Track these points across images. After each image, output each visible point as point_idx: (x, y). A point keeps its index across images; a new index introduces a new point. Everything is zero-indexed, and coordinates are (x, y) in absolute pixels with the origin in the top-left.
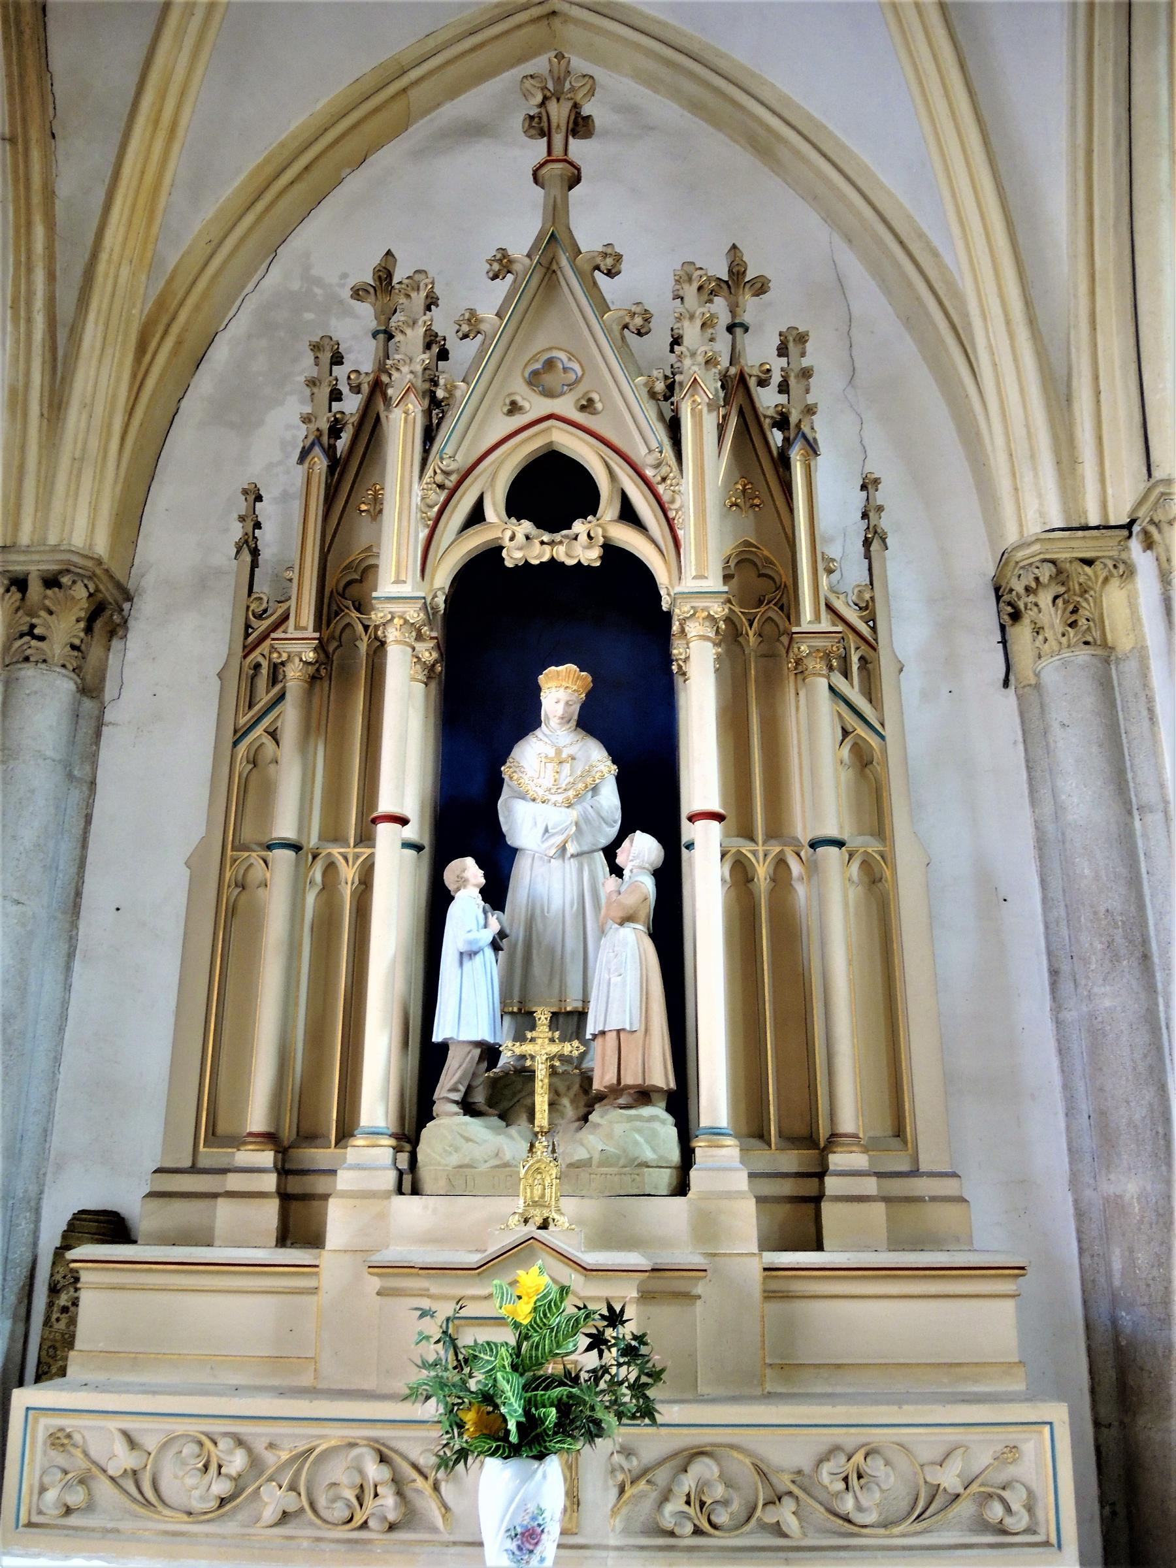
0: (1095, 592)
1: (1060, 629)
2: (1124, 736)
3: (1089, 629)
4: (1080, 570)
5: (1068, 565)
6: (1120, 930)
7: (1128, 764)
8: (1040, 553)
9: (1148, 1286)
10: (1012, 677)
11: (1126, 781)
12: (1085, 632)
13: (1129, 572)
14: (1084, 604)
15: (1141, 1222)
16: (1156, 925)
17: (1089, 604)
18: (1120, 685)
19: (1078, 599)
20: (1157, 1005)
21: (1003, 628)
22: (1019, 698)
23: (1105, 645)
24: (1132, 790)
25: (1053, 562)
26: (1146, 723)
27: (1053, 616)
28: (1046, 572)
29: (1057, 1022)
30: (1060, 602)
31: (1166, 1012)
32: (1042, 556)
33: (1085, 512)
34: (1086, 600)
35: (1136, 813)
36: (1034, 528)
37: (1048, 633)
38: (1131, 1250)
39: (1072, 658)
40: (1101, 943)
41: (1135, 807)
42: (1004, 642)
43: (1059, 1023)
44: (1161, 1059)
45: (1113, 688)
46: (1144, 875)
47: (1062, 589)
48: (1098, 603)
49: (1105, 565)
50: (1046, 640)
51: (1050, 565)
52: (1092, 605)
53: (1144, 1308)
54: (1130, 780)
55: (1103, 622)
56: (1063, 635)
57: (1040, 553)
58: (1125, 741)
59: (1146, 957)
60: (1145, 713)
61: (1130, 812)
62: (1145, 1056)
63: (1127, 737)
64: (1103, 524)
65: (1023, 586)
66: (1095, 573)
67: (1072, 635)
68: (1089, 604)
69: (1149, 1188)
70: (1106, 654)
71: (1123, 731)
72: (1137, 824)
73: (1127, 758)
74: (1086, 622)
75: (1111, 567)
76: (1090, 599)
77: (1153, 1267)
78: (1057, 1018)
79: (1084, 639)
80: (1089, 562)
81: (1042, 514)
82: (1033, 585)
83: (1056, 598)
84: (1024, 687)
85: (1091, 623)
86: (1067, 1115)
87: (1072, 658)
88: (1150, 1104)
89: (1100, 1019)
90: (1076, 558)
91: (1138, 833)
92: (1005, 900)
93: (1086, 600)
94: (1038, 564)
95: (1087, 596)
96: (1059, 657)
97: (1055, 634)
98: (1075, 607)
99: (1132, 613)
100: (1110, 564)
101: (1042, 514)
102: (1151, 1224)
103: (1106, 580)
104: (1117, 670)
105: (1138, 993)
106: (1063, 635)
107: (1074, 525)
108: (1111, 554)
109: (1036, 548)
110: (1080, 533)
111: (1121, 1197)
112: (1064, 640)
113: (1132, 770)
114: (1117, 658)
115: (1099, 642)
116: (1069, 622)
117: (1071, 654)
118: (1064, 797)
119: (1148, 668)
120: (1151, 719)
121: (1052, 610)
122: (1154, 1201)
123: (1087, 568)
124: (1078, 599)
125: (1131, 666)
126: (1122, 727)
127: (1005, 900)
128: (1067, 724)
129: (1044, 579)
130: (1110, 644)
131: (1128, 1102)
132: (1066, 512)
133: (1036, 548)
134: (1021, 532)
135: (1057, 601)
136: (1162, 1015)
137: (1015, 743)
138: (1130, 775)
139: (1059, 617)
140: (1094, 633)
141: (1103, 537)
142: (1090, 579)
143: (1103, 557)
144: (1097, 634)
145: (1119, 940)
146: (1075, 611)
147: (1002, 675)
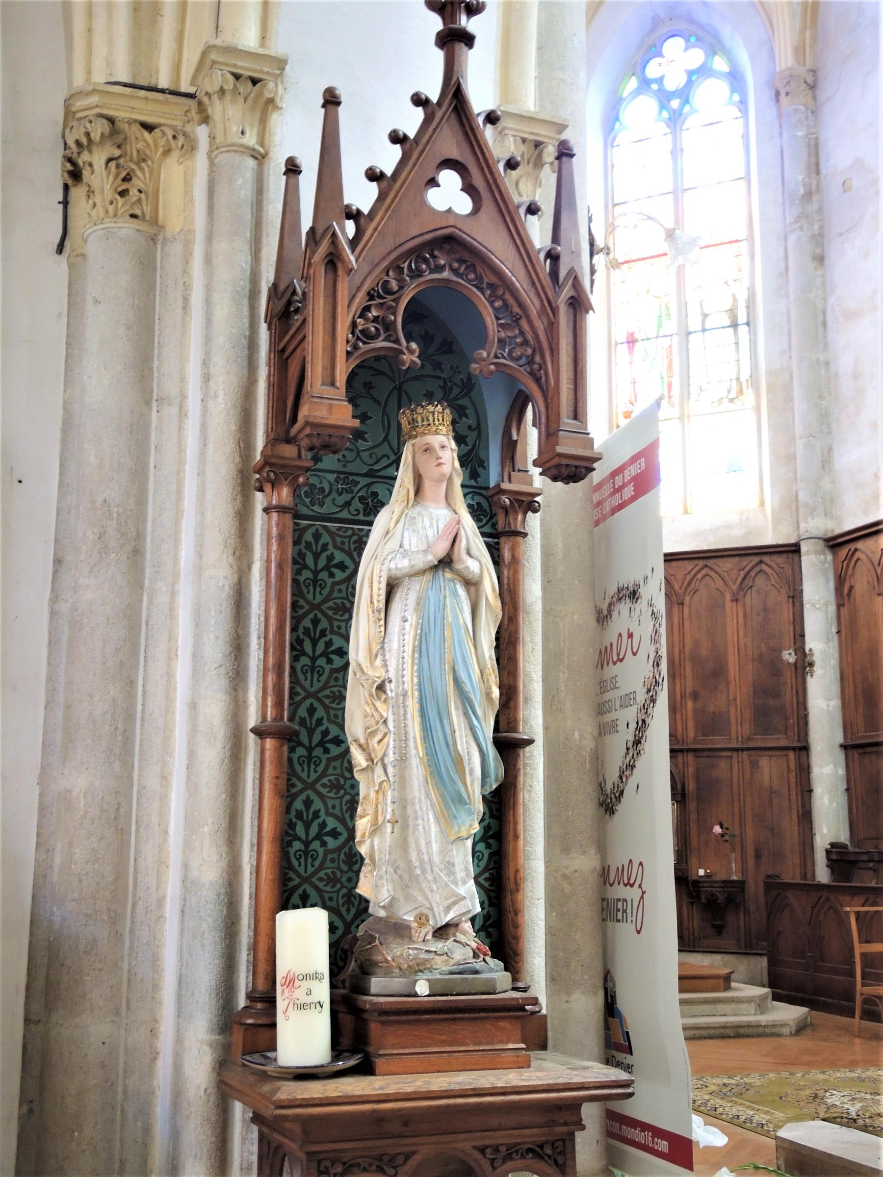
0: (153, 163)
1: (109, 194)
2: (157, 322)
3: (139, 200)
4: (139, 136)
5: (126, 126)
6: (115, 521)
7: (156, 352)
8: (97, 106)
9: (81, 881)
10: (67, 244)
11: (151, 370)
12: (134, 203)
13: (190, 147)
14: (139, 173)
15: (84, 817)
16: (154, 520)
17: (144, 174)
18: (162, 267)
19: (134, 166)
20: (140, 601)
21: (66, 188)
22: (71, 266)
23: (154, 221)
24: (155, 379)
25: (111, 120)
26: (179, 311)
27: (105, 180)
28: (99, 129)
29: (51, 613)
30: (113, 164)
31: (148, 609)
32: (98, 110)
33: (157, 72)
34: (141, 169)
35: (154, 404)
36: (99, 78)
37: (98, 199)
38: (70, 845)
39: (115, 230)
40: (94, 533)
41: (155, 397)
42: (65, 203)
43: (53, 614)
44: (135, 653)
45: (155, 269)
46: (152, 469)
47: (117, 153)
48: (155, 176)
49: (164, 133)
50: (95, 205)
51: (105, 121)
52: (147, 175)
53: (74, 903)
54: (155, 369)
55: (157, 197)
56: (111, 203)
57: (97, 106)
58: (157, 327)
59: (137, 552)
60: (180, 302)
61: (148, 403)
62: (118, 651)
63: (160, 324)
64: (172, 88)
65: (74, 140)
66: (155, 141)
67: (120, 204)
68: (144, 174)
69: (97, 783)
70: (154, 232)
71: (157, 317)
72: (154, 416)
73: (156, 345)
74: (137, 193)
75: (170, 137)
76: (146, 169)
77: (87, 862)
78: (52, 609)
79: (132, 212)
80: (149, 127)
81: (109, 64)
82: (84, 141)
83: (110, 160)
84: (77, 255)
85: (143, 196)
86: (46, 707)
87: (115, 230)
88: (114, 699)
89: (80, 611)
90: (135, 121)
91: (154, 424)
92: (20, 482)
93: (141, 169)
94: (92, 118)
95: (143, 165)
96: (101, 226)
97: (103, 200)
98: (128, 174)
99: (186, 192)
100: (170, 133)
101: (109, 64)
102: (93, 820)
103: (167, 152)
104: (162, 250)
105: (121, 587)
106: (111, 203)
107: (142, 83)
108: (175, 123)
109: (94, 99)
110: (143, 93)
111: (69, 791)
112: (111, 209)
113: (159, 359)
114: (165, 238)
115: (147, 218)
116: (120, 189)
117: (113, 225)
118: (85, 378)
119: (191, 254)
120: (184, 308)
121: (104, 173)
122: (100, 796)
123: (146, 134)
124: (134, 166)
125: (176, 249)
126: (157, 312)
127: (20, 482)
128: (99, 300)
129: (96, 136)
130: (160, 222)
131: (91, 696)
132: (134, 65)
133: (94, 99)
134: (88, 81)
135: (110, 164)
136: (144, 612)
137: (60, 315)
138: (156, 364)
139: (110, 182)
140: (145, 207)
141: (167, 103)
142: (148, 145)
143: (164, 125)
144: (148, 209)
145: (111, 531)
146: (127, 179)
147: (57, 240)
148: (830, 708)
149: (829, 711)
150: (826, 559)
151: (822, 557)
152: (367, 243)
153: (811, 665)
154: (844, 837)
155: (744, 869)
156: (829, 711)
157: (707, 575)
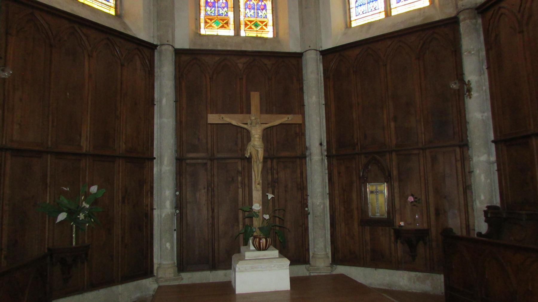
148: (484, 118)
149: (483, 120)
150: (477, 22)
151: (474, 21)
152: (326, 273)
153: (469, 90)
154: (497, 201)
155: (429, 223)
156: (483, 120)
157: (400, 46)
